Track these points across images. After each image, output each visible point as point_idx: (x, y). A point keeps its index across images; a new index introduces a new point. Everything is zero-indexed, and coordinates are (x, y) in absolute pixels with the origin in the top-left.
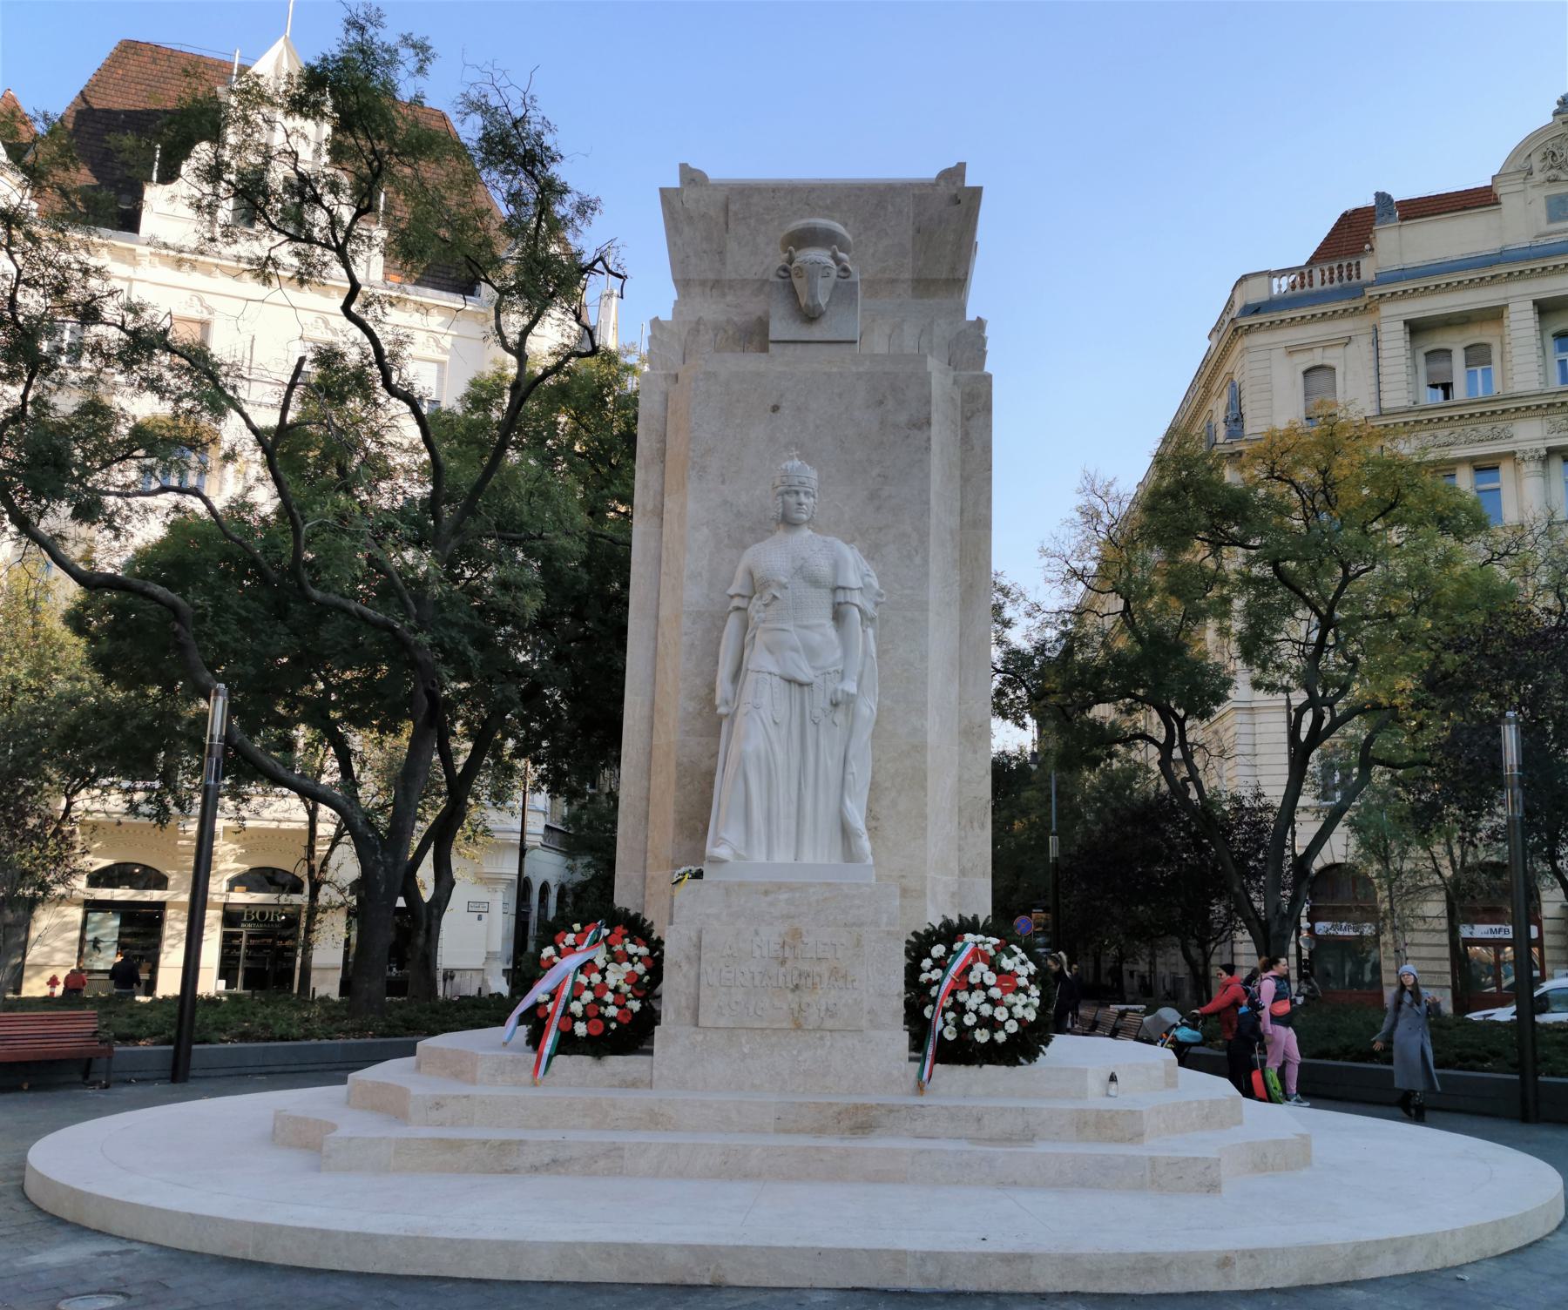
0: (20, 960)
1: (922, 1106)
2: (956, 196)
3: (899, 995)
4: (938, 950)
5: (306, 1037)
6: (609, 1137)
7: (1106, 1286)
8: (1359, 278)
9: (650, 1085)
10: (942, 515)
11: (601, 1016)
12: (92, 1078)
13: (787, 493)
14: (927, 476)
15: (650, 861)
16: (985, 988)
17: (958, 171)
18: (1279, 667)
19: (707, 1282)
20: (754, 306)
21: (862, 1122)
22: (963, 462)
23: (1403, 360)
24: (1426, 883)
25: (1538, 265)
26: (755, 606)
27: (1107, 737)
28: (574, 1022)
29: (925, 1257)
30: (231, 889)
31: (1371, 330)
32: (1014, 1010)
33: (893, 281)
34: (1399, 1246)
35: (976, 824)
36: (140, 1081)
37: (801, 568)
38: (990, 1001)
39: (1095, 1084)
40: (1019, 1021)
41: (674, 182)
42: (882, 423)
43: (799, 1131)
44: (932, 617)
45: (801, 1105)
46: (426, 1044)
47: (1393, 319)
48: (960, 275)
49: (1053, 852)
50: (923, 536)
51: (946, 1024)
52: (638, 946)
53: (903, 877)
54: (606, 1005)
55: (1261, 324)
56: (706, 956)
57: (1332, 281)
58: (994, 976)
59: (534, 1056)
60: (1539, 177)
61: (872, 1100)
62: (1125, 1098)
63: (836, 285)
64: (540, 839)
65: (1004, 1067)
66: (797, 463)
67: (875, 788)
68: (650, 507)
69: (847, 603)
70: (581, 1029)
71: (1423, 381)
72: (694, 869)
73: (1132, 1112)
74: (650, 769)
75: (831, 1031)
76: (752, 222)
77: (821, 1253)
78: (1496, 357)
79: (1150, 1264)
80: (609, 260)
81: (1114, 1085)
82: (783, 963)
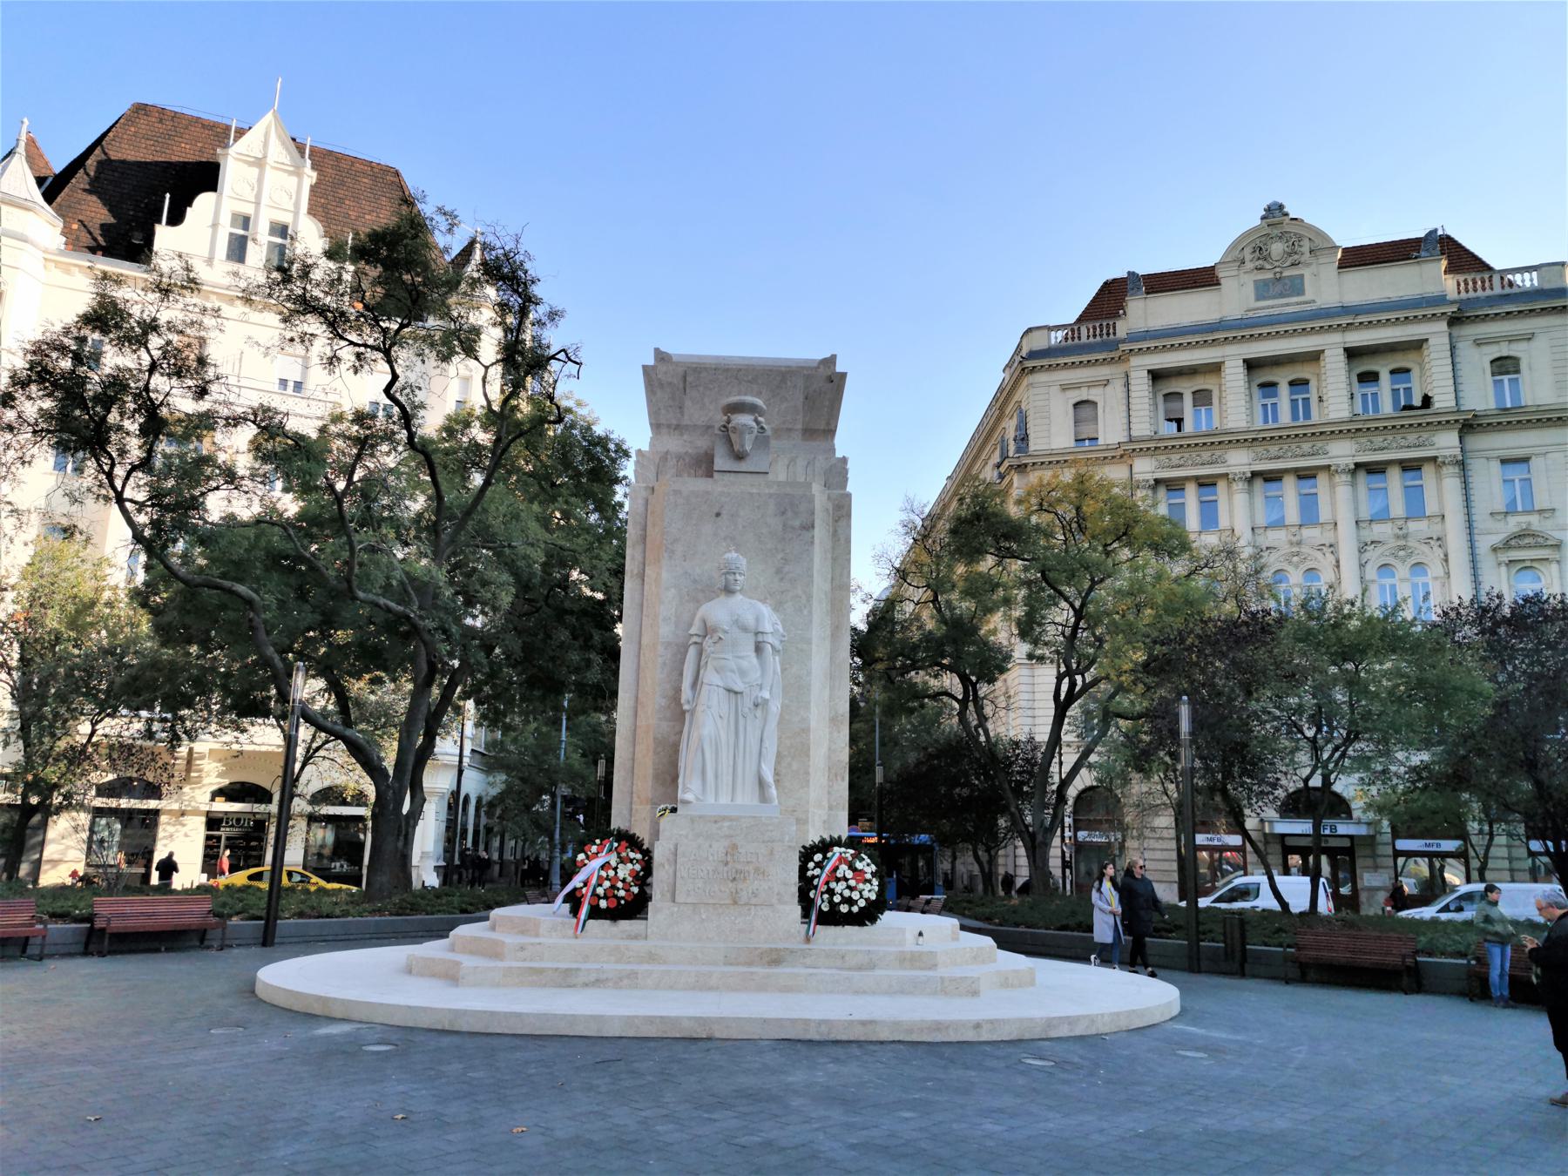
0: (37, 856)
4: (818, 857)
5: (343, 916)
6: (629, 967)
7: (914, 1038)
9: (646, 938)
10: (821, 584)
11: (615, 896)
12: (206, 943)
14: (812, 560)
15: (635, 799)
16: (846, 880)
17: (831, 361)
18: (1046, 644)
20: (702, 443)
21: (775, 958)
22: (833, 548)
23: (1147, 400)
24: (1159, 802)
25: (1247, 333)
26: (708, 643)
27: (919, 694)
29: (820, 1023)
30: (213, 800)
33: (789, 430)
34: (1071, 1020)
36: (239, 945)
38: (849, 887)
39: (910, 936)
41: (651, 361)
43: (738, 964)
46: (497, 913)
47: (1140, 367)
48: (832, 427)
49: (879, 778)
50: (809, 598)
54: (618, 889)
57: (1095, 336)
60: (1249, 265)
61: (780, 945)
62: (927, 944)
66: (734, 555)
67: (779, 756)
68: (635, 572)
70: (603, 904)
71: (1161, 416)
72: (670, 807)
76: (701, 389)
78: (1215, 400)
82: (726, 864)
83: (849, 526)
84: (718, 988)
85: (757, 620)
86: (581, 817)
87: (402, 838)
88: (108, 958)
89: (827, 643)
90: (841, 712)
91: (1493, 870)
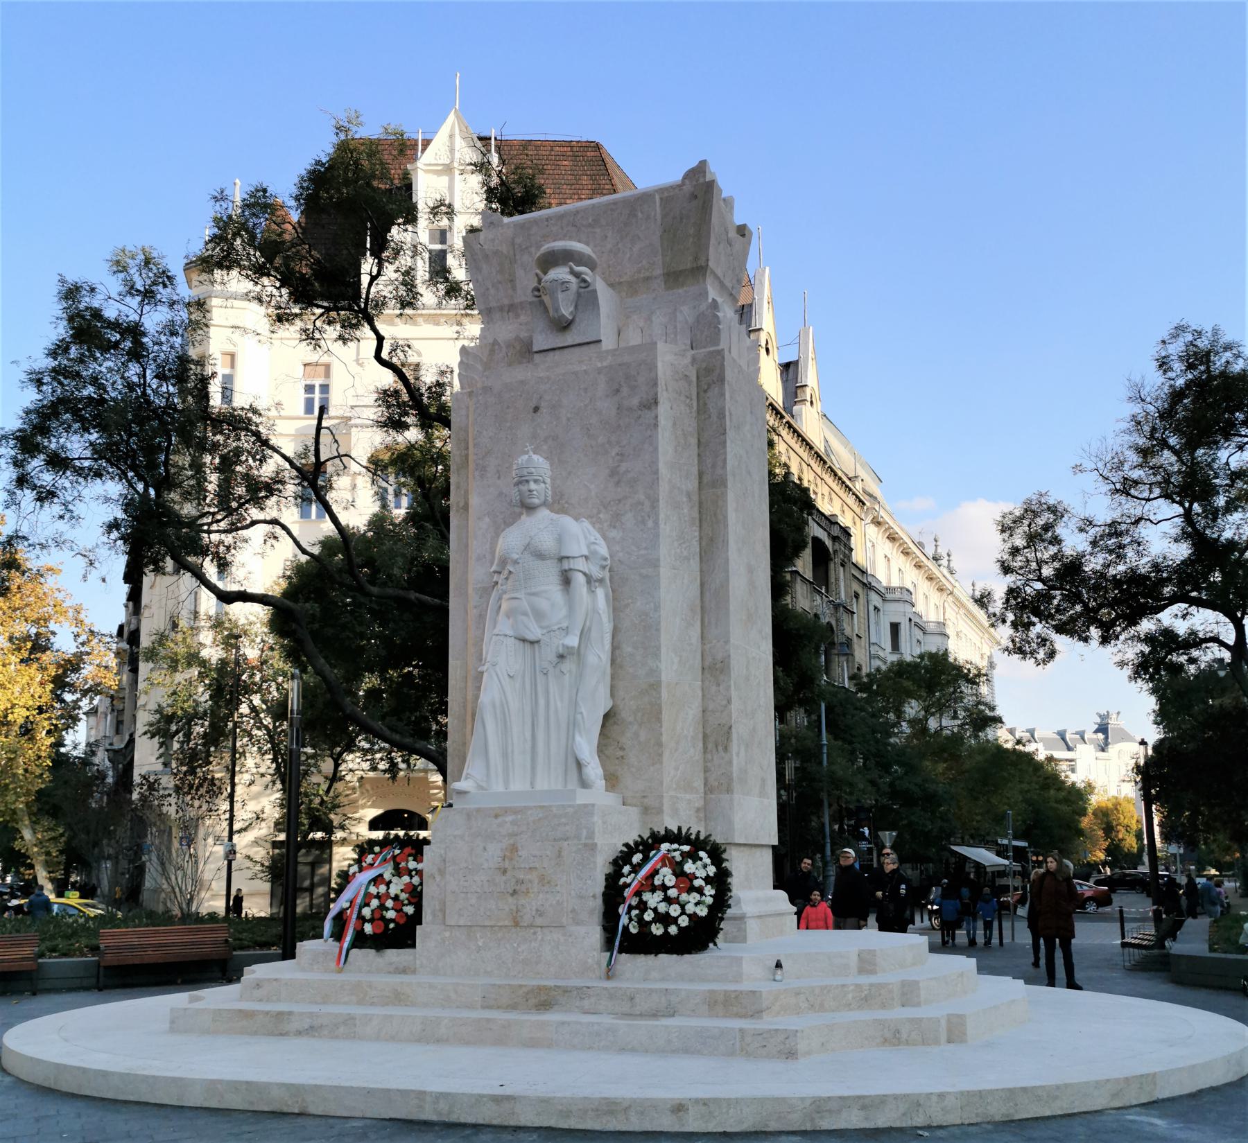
1: (588, 988)
2: (693, 193)
4: (637, 858)
7: (573, 1123)
11: (383, 918)
19: (296, 1111)
32: (687, 907)
33: (648, 279)
35: (720, 748)
40: (689, 916)
44: (665, 572)
45: (500, 986)
50: (654, 502)
51: (631, 919)
53: (644, 797)
54: (387, 909)
58: (674, 879)
63: (579, 295)
65: (675, 956)
69: (571, 570)
70: (368, 928)
73: (754, 992)
75: (541, 927)
77: (370, 1092)
79: (610, 1107)
81: (779, 972)
82: (505, 872)
84: (447, 1040)
85: (560, 540)
86: (866, 830)
88: (105, 992)
89: (695, 564)
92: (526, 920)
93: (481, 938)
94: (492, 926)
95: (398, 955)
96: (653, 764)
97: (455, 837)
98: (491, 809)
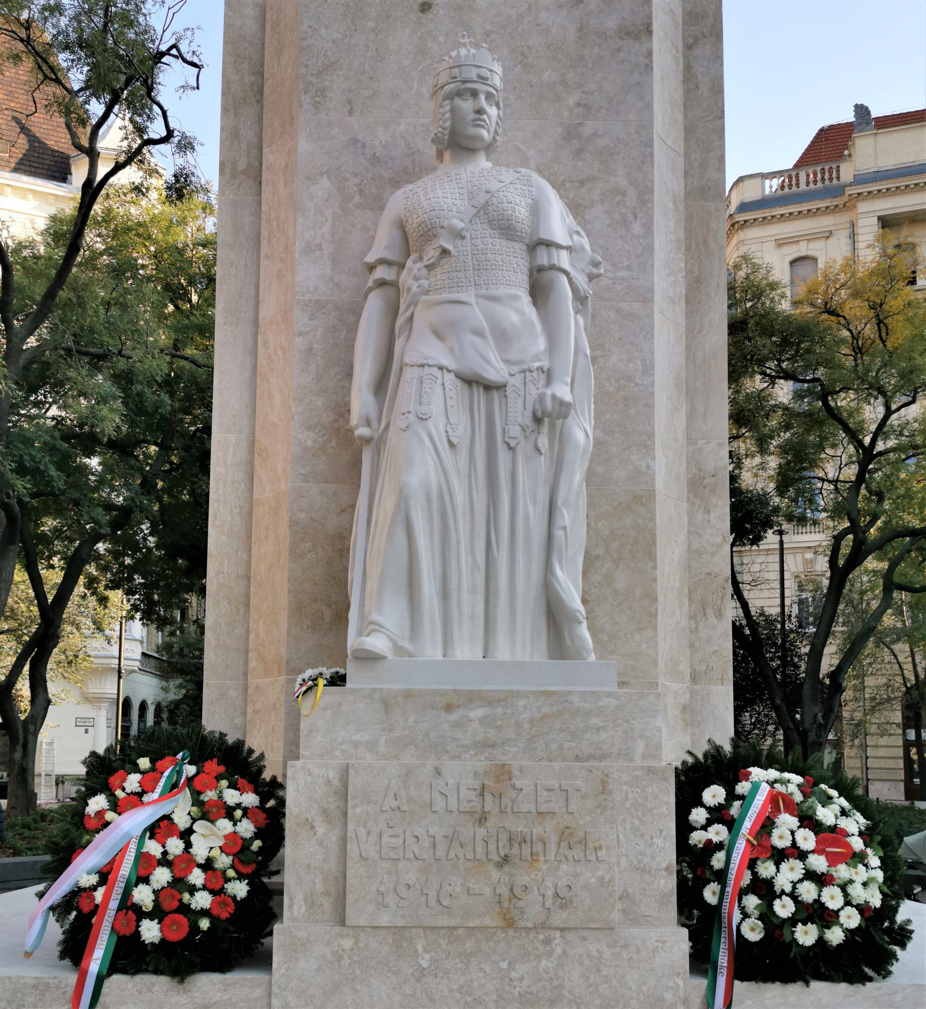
3: (667, 869)
4: (714, 794)
8: (838, 178)
11: (184, 909)
13: (459, 94)
14: (649, 107)
15: (253, 664)
16: (802, 855)
22: (459, 707)
28: (139, 920)
31: (848, 226)
35: (710, 612)
37: (486, 205)
38: (810, 875)
42: (580, 30)
50: (645, 193)
51: (745, 915)
52: (242, 791)
54: (192, 890)
55: (755, 220)
56: (356, 810)
57: (815, 182)
58: (811, 835)
59: (72, 978)
64: (138, 664)
65: (844, 985)
70: (150, 931)
72: (328, 672)
74: (249, 537)
75: (562, 930)
80: (184, 47)
82: (482, 819)
83: (718, 58)
87: (19, 748)
89: (681, 308)
90: (710, 466)
91: (898, 747)
92: (533, 911)
93: (426, 951)
94: (450, 928)
95: (226, 987)
96: (640, 630)
97: (356, 745)
98: (436, 692)
